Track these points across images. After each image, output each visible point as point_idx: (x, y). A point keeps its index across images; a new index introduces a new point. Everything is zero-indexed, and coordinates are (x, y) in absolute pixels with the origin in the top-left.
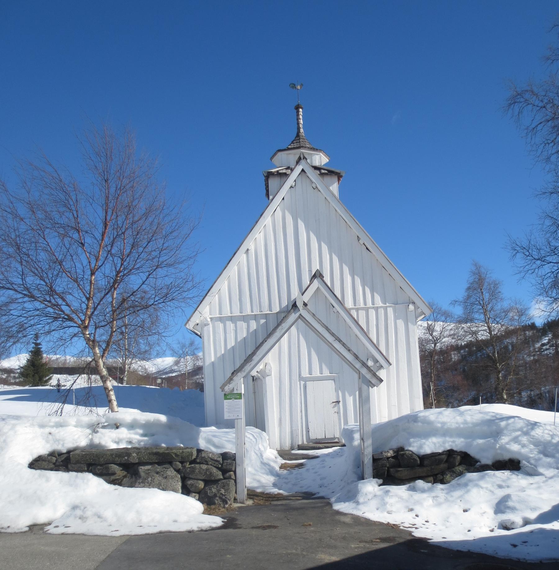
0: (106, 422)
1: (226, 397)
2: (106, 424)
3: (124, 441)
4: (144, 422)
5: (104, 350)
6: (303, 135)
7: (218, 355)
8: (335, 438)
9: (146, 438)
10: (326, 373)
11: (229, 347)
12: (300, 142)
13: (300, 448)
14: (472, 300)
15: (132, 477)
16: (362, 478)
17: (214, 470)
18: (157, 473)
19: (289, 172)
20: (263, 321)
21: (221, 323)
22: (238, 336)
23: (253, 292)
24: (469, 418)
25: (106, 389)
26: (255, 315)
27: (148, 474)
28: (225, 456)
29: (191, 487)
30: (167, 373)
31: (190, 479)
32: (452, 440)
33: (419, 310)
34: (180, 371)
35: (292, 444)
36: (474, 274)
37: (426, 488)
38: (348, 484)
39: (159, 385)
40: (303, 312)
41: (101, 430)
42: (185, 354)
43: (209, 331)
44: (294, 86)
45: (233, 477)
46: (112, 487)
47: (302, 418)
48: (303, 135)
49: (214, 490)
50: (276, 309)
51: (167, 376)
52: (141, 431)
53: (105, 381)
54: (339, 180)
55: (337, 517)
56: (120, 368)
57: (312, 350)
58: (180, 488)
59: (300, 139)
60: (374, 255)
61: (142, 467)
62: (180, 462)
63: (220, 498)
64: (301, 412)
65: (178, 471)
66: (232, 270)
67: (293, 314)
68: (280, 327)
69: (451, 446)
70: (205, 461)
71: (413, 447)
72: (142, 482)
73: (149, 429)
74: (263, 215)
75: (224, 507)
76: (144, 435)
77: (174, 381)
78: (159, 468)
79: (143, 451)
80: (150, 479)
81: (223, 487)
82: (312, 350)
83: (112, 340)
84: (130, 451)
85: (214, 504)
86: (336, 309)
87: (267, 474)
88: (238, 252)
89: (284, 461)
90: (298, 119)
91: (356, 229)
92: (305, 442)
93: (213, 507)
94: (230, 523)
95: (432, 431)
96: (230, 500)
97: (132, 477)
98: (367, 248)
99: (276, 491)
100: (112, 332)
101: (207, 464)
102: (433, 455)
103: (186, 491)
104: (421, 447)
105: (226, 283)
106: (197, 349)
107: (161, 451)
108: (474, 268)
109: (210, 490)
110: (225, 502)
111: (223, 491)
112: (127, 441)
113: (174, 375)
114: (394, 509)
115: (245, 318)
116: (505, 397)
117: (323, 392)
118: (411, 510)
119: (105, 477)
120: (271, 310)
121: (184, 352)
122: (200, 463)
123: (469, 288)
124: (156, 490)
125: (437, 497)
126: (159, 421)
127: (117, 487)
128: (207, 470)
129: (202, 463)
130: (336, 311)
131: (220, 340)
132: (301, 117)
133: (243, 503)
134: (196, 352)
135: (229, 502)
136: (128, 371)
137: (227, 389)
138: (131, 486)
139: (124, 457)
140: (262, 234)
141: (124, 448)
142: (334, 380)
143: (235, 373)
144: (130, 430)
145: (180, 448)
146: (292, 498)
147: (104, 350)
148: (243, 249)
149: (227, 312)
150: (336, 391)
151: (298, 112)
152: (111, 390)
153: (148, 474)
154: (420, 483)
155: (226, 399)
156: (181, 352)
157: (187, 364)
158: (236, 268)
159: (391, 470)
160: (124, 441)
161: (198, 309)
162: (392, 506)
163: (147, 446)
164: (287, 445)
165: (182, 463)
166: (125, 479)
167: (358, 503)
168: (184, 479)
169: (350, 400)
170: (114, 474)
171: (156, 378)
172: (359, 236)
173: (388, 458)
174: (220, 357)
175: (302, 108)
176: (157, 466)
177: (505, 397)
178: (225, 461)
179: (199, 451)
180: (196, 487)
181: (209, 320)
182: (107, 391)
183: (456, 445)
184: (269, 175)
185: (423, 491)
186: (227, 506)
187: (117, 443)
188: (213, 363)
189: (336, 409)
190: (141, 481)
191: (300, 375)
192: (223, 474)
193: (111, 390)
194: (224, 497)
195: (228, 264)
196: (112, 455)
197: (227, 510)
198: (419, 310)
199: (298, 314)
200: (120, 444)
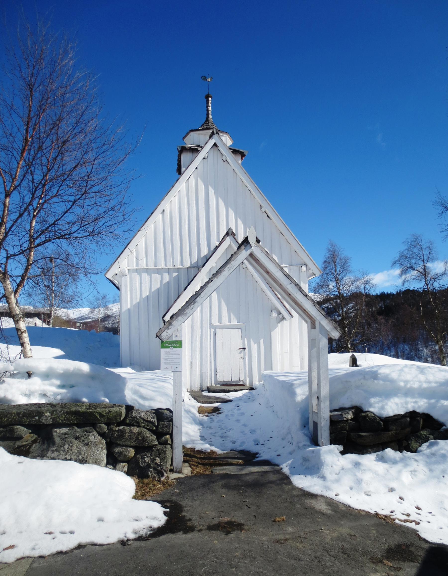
0: (15, 370)
1: (163, 344)
2: (15, 372)
3: (36, 394)
4: (62, 372)
5: (19, 285)
6: (212, 120)
7: (134, 303)
8: (240, 381)
9: (63, 391)
10: (234, 322)
11: (144, 296)
12: (209, 125)
13: (209, 390)
14: (327, 271)
15: (43, 443)
16: (315, 442)
17: (148, 434)
18: (77, 438)
19: (199, 149)
20: (175, 274)
21: (138, 274)
22: (153, 286)
23: (167, 248)
24: (431, 378)
25: (18, 330)
26: (168, 269)
27: (64, 439)
28: (158, 413)
29: (119, 456)
30: (83, 319)
31: (118, 445)
32: (414, 400)
33: (311, 272)
34: (93, 318)
35: (201, 386)
36: (330, 251)
37: (398, 459)
38: (299, 448)
39: (78, 327)
40: (255, 250)
41: (7, 380)
42: (99, 306)
43: (126, 281)
44: (205, 78)
45: (169, 442)
46: (16, 458)
47: (211, 363)
48: (212, 120)
49: (147, 459)
50: (187, 264)
51: (83, 321)
52: (58, 382)
53: (18, 321)
54: (242, 159)
55: (309, 502)
56: (48, 314)
57: (222, 300)
58: (105, 457)
59: (209, 123)
60: (274, 222)
61: (58, 430)
62: (105, 424)
63: (154, 469)
64: (211, 356)
65: (102, 435)
66: (150, 226)
67: (244, 251)
68: (229, 266)
69: (413, 407)
70: (136, 422)
71: (374, 407)
72: (57, 450)
73: (68, 380)
74: (179, 181)
75: (159, 481)
76: (62, 386)
77: (89, 325)
78: (79, 431)
79: (59, 410)
80: (66, 447)
81: (159, 455)
82: (222, 300)
83: (28, 275)
84: (43, 409)
85: (147, 477)
86: (245, 265)
87: (191, 423)
88: (155, 211)
89: (199, 405)
90: (207, 107)
91: (259, 198)
92: (213, 384)
93: (146, 481)
94: (176, 521)
95: (392, 390)
96: (166, 472)
97: (43, 443)
98: (268, 216)
99: (207, 447)
100: (28, 265)
101: (139, 426)
102: (397, 418)
103: (113, 461)
104: (383, 408)
105: (143, 239)
106: (108, 302)
107: (82, 409)
108: (330, 247)
109: (143, 458)
110: (161, 474)
111: (158, 461)
112: (40, 394)
113: (89, 320)
114: (371, 488)
115: (159, 271)
116: (349, 346)
117: (232, 339)
118: (392, 490)
119: (8, 443)
120: (182, 264)
121: (97, 303)
122: (130, 425)
123: (325, 262)
124: (73, 463)
125: (415, 471)
126: (80, 370)
127: (22, 458)
128: (139, 433)
129: (133, 425)
130: (245, 267)
131: (137, 290)
132: (210, 105)
133: (180, 472)
134: (107, 304)
135: (165, 475)
136: (54, 316)
137: (164, 335)
138: (42, 456)
139: (34, 417)
140: (177, 198)
141: (35, 404)
142: (241, 329)
143: (175, 317)
144: (45, 380)
145: (106, 406)
146: (230, 461)
147: (19, 285)
148: (160, 209)
149: (143, 265)
150: (243, 338)
151: (208, 100)
152: (25, 332)
153: (64, 439)
154: (389, 452)
155: (163, 347)
156: (96, 304)
157: (99, 314)
158: (153, 226)
159: (352, 434)
160: (36, 394)
161: (128, 247)
162: (367, 484)
163: (65, 401)
164: (197, 387)
165: (108, 424)
166: (34, 445)
167: (323, 478)
168: (110, 446)
169: (254, 347)
170: (20, 438)
171: (75, 323)
172: (262, 204)
173: (347, 420)
174: (135, 304)
175: (211, 97)
176: (76, 428)
177: (349, 346)
178: (161, 422)
179: (129, 408)
180: (125, 455)
181: (127, 271)
182: (19, 333)
183: (419, 407)
184: (183, 150)
185: (395, 462)
186: (162, 479)
187: (28, 396)
188: (129, 310)
189: (242, 355)
190: (54, 449)
191: (210, 323)
192: (158, 439)
193: (25, 332)
194: (159, 468)
195: (146, 222)
196: (18, 414)
197: (164, 485)
198: (311, 272)
199: (249, 252)
200: (32, 397)
